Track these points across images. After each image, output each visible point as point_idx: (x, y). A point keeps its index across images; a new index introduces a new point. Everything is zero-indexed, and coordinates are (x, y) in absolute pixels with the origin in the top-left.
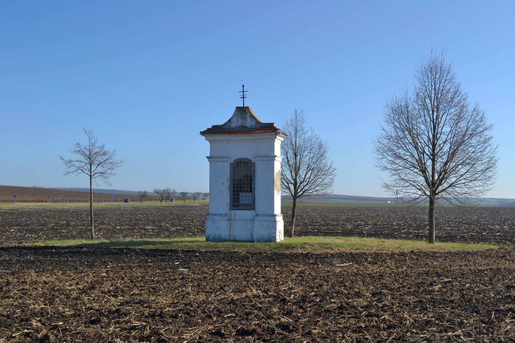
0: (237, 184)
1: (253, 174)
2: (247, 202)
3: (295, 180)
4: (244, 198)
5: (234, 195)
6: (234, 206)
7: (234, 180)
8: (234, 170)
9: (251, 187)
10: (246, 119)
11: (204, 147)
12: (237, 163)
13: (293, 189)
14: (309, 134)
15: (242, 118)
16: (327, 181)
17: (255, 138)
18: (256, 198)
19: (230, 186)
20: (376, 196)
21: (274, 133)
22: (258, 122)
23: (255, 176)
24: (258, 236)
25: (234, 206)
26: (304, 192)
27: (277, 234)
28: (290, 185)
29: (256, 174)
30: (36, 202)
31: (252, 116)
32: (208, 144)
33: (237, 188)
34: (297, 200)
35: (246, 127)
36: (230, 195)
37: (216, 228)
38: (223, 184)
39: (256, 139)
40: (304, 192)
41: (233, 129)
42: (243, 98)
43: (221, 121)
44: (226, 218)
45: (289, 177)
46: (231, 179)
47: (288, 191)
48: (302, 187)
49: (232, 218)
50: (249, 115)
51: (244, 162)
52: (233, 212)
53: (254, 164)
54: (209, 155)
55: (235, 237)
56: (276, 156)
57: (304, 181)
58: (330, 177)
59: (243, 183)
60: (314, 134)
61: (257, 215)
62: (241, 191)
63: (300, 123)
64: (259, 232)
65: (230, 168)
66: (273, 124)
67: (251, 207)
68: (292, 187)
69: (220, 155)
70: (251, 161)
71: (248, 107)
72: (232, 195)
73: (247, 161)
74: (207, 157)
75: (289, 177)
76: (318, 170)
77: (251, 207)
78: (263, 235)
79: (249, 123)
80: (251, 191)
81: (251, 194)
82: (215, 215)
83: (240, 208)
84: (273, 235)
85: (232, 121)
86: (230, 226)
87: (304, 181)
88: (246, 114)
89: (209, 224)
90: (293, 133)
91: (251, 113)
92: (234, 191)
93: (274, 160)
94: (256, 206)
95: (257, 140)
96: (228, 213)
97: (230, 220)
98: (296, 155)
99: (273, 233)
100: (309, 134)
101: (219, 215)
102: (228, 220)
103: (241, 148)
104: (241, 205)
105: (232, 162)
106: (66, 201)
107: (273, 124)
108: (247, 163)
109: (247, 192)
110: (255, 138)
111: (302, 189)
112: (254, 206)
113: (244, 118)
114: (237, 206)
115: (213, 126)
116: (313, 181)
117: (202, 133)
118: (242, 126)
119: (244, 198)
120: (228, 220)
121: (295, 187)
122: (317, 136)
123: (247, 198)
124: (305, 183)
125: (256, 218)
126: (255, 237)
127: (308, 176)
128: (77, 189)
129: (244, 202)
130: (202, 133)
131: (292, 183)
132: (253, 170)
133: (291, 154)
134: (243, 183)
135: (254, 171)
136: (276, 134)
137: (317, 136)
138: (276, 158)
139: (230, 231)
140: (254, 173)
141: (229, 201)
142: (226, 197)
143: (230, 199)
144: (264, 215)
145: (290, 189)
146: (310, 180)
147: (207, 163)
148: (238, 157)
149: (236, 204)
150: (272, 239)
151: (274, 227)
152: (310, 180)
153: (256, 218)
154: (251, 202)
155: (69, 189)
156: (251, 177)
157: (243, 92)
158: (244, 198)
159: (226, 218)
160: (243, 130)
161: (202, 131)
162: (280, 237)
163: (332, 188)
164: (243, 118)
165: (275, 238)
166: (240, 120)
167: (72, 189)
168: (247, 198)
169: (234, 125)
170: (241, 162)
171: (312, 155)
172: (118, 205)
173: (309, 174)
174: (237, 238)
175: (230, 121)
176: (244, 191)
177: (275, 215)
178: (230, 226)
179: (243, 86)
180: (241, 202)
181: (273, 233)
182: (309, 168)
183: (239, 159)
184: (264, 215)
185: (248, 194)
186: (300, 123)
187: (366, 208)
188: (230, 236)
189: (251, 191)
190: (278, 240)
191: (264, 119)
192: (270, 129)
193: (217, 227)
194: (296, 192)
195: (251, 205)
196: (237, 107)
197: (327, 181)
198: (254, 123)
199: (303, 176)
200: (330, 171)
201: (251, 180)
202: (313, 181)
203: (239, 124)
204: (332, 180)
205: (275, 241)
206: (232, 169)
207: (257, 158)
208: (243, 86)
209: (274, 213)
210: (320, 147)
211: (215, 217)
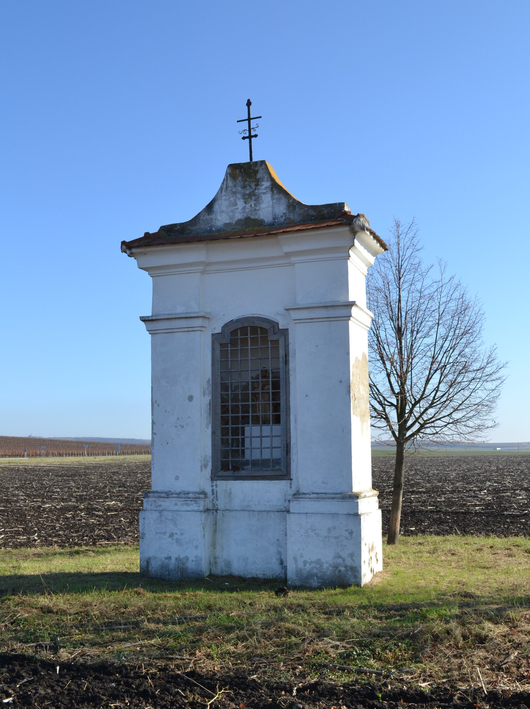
0: (235, 399)
1: (281, 365)
2: (266, 455)
3: (402, 396)
4: (258, 440)
5: (225, 432)
6: (225, 467)
7: (224, 387)
8: (223, 353)
9: (277, 407)
10: (258, 199)
11: (136, 288)
12: (234, 333)
13: (396, 420)
14: (434, 275)
15: (247, 198)
16: (481, 394)
17: (287, 249)
18: (293, 441)
19: (212, 404)
20: (498, 442)
21: (346, 229)
22: (294, 205)
23: (287, 372)
24: (301, 565)
25: (225, 467)
26: (422, 426)
27: (365, 555)
28: (388, 409)
29: (291, 365)
30: (9, 456)
31: (276, 188)
32: (146, 280)
33: (235, 409)
34: (407, 445)
35: (259, 223)
36: (213, 433)
37: (172, 535)
38: (191, 398)
39: (288, 255)
40: (422, 426)
41: (219, 230)
42: (250, 137)
43: (182, 214)
44: (201, 505)
45: (384, 388)
46: (214, 385)
47: (383, 423)
48: (417, 415)
49: (221, 504)
50: (266, 184)
51: (254, 330)
52: (222, 485)
53: (285, 332)
54: (148, 313)
55: (228, 564)
56: (353, 304)
57: (421, 398)
58: (490, 385)
59: (250, 394)
60: (446, 277)
61: (297, 495)
62: (245, 420)
63: (409, 251)
64: (306, 551)
65: (213, 349)
66: (342, 205)
67: (278, 468)
68: (393, 414)
69: (180, 310)
70: (274, 325)
71: (263, 162)
72: (219, 432)
73: (265, 325)
74: (144, 320)
75: (384, 388)
76: (457, 369)
77: (278, 468)
78: (318, 562)
79: (268, 209)
80: (277, 420)
81: (277, 429)
82: (168, 495)
83: (243, 473)
84: (349, 562)
85: (216, 207)
86: (215, 531)
87: (421, 398)
88: (258, 183)
89: (148, 520)
90: (391, 277)
91: (273, 180)
92: (224, 421)
93: (349, 316)
94: (293, 465)
95: (293, 259)
96: (208, 490)
97: (211, 510)
98: (399, 332)
99: (352, 555)
100: (434, 275)
101: (179, 495)
102: (207, 510)
103: (245, 286)
104: (247, 463)
105: (219, 330)
106: (53, 455)
107: (342, 205)
108: (264, 331)
109: (266, 422)
110: (287, 249)
111: (417, 419)
112: (288, 465)
113: (250, 195)
114: (236, 468)
115: (163, 228)
116: (444, 399)
117: (128, 247)
118: (248, 219)
119: (258, 440)
120: (207, 510)
121: (401, 415)
122: (456, 281)
123: (266, 442)
124: (424, 404)
125: (294, 507)
126: (291, 574)
127: (431, 386)
128: (84, 438)
129: (256, 455)
130: (128, 247)
131: (392, 405)
132: (282, 352)
133: (388, 333)
134: (250, 394)
135: (286, 356)
136: (354, 233)
137: (456, 281)
138: (354, 310)
139: (214, 545)
140: (286, 362)
141: (209, 452)
142: (199, 439)
143: (214, 445)
144: (321, 496)
145: (387, 419)
146: (439, 394)
147: (144, 338)
148: (234, 316)
149: (230, 461)
150: (345, 578)
151: (354, 535)
152: (439, 394)
153: (294, 507)
154: (277, 454)
155: (75, 438)
156: (276, 375)
157: (249, 119)
158: (256, 443)
159: (201, 505)
160: (251, 230)
161: (127, 240)
162: (373, 559)
163: (493, 415)
164: (251, 196)
165: (356, 571)
166: (241, 204)
167: (79, 438)
168: (266, 442)
169: (222, 218)
170: (244, 330)
171: (442, 331)
172: (124, 459)
173: (436, 377)
174: (238, 568)
175: (210, 208)
176: (256, 421)
177: (357, 496)
178: (215, 531)
179: (249, 104)
180: (247, 456)
181: (352, 555)
182: (436, 366)
183: (238, 321)
184: (321, 496)
185: (266, 430)
186: (409, 251)
187: (475, 458)
188: (213, 561)
189: (277, 420)
190: (366, 578)
191: (311, 194)
192: (335, 219)
193: (175, 536)
194: (403, 428)
195: (277, 462)
196: (230, 166)
197: (481, 394)
198: (281, 209)
199: (421, 384)
200: (488, 370)
201: (276, 385)
202: (444, 399)
203: (239, 216)
204: (493, 394)
205: (358, 585)
206: (218, 352)
207: (295, 315)
208: (249, 104)
209: (351, 488)
210: (462, 311)
211: (167, 503)
